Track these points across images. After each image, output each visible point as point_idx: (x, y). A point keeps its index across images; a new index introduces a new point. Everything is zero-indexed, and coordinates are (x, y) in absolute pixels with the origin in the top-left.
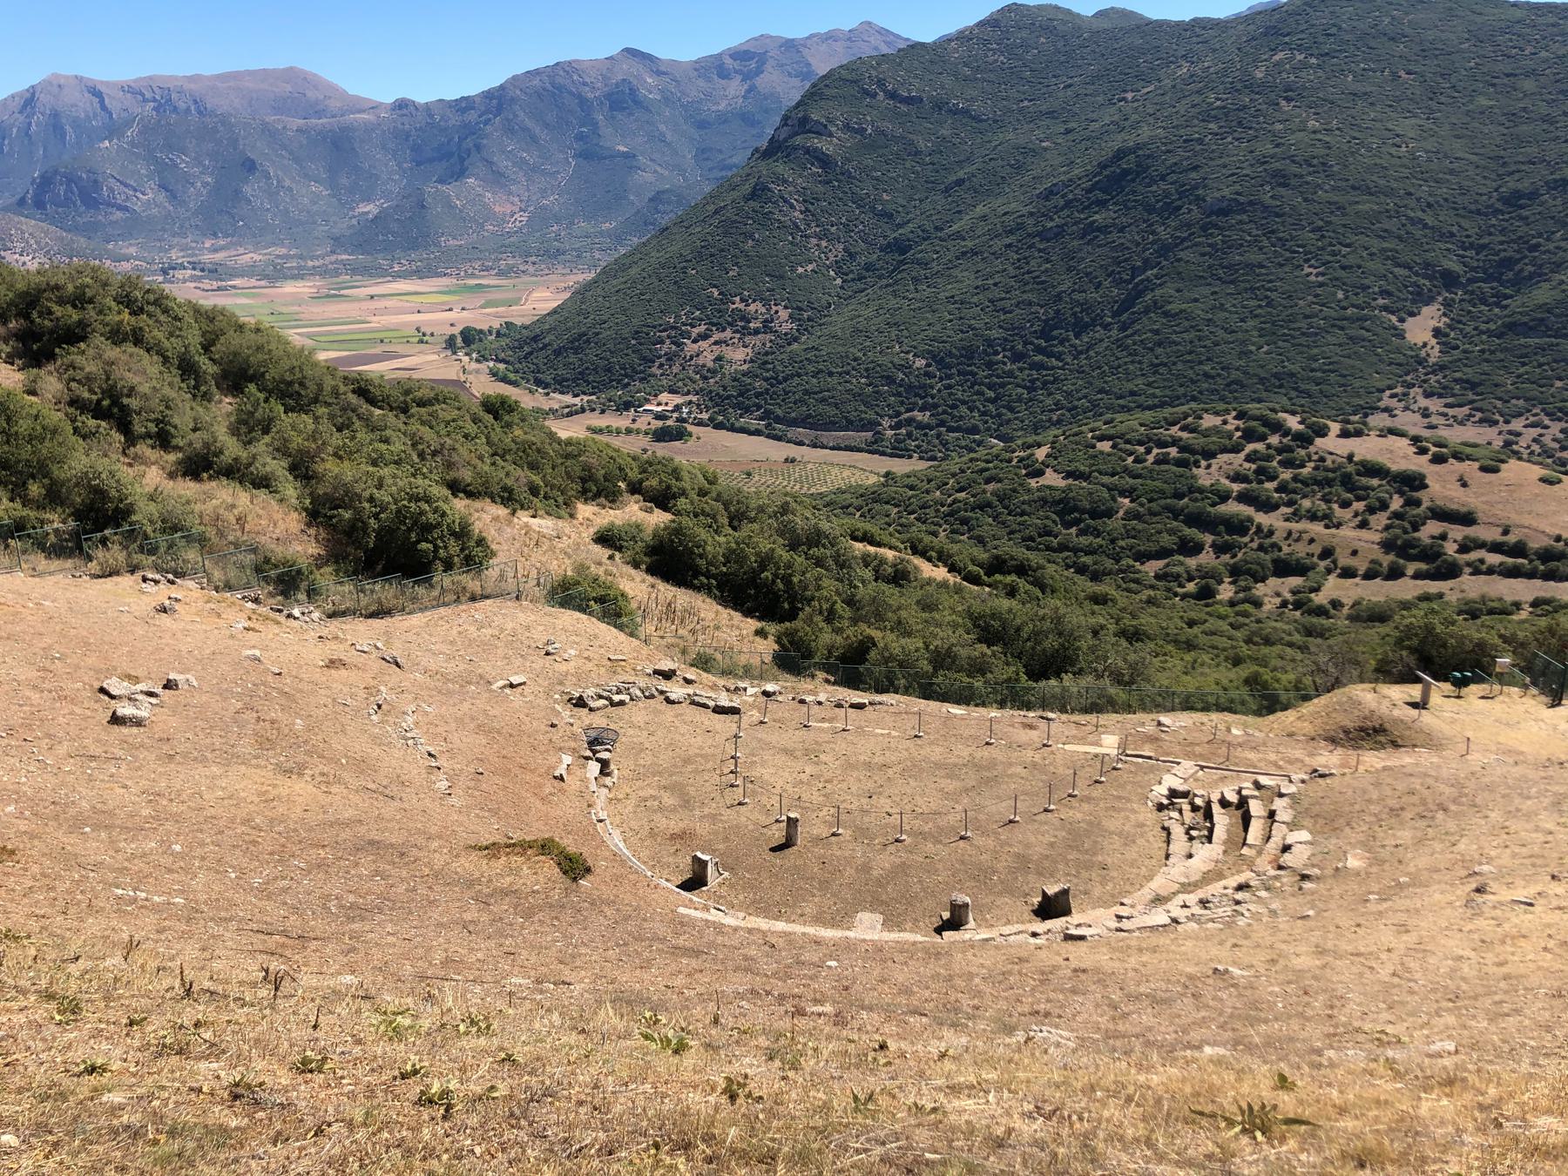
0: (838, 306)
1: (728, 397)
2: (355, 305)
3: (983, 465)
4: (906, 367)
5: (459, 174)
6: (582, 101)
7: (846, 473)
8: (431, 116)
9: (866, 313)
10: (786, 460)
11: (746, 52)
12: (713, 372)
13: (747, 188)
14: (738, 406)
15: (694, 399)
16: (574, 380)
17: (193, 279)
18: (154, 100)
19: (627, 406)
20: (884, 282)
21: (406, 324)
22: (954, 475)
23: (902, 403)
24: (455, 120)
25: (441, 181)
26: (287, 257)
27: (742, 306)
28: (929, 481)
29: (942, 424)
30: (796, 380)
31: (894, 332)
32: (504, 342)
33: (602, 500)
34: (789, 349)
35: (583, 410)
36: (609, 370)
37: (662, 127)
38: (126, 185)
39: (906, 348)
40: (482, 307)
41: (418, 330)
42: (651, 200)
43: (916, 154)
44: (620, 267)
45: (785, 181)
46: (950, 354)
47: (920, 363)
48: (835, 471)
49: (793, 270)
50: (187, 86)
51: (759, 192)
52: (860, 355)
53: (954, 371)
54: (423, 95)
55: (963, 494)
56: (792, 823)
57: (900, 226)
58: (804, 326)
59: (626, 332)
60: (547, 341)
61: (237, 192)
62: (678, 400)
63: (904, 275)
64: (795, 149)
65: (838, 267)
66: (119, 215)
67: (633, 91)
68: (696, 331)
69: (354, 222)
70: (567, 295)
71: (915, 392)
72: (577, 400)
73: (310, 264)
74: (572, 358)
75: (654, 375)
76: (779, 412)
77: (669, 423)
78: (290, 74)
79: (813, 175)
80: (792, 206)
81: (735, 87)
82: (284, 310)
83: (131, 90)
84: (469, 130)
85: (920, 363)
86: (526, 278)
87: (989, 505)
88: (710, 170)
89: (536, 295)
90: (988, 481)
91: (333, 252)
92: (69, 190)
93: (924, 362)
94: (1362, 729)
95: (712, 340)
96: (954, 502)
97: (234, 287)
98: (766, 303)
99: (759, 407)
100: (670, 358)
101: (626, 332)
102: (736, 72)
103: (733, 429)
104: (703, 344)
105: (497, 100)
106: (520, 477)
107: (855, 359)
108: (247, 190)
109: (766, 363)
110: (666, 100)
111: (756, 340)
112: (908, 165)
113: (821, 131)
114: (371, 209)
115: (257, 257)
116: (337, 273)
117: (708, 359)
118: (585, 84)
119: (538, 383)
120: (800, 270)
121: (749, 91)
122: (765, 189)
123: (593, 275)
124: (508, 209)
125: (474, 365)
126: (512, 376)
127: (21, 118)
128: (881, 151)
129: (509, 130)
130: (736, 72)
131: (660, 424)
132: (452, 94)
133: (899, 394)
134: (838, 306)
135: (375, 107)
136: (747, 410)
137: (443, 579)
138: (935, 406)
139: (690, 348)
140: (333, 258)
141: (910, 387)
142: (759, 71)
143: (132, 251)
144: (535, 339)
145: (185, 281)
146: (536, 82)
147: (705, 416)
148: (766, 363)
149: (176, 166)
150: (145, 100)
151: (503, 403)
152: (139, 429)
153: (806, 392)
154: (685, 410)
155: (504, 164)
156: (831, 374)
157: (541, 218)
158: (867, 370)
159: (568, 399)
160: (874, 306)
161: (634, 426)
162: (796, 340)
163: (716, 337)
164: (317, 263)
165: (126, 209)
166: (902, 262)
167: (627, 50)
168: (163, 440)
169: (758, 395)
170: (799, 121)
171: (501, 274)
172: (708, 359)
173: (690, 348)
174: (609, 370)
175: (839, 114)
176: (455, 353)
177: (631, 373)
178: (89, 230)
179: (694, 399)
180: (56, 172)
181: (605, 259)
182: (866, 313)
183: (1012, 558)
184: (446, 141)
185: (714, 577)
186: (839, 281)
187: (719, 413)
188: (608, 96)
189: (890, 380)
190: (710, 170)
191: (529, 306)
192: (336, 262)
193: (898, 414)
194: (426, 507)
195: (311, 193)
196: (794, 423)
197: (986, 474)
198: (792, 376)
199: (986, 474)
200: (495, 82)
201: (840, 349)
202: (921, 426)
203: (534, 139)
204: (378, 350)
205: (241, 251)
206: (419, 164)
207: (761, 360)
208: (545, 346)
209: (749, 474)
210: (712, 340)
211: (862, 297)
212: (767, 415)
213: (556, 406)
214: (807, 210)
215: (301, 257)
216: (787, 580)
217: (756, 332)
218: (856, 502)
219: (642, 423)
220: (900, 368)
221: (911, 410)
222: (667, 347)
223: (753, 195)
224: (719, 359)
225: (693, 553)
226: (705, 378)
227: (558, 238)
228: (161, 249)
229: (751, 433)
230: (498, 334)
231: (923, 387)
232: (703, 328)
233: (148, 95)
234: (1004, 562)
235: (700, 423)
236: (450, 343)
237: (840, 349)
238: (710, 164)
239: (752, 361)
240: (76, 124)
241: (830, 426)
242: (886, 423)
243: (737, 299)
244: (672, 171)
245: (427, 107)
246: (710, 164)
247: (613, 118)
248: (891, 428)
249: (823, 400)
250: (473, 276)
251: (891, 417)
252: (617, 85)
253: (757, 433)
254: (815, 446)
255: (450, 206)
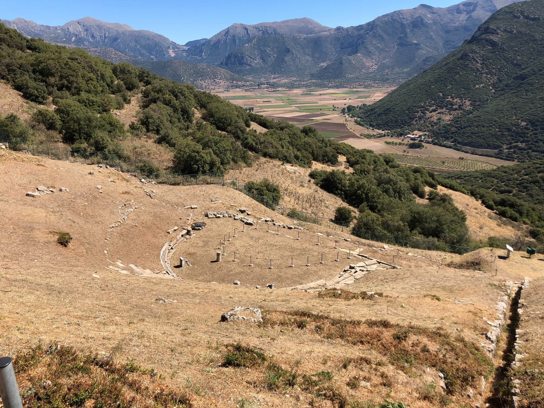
0: (491, 100)
1: (440, 133)
2: (315, 97)
3: (538, 165)
4: (517, 125)
5: (356, 52)
6: (402, 25)
7: (484, 165)
8: (348, 32)
9: (504, 103)
10: (460, 158)
11: (469, 3)
12: (436, 124)
13: (459, 56)
14: (444, 137)
15: (427, 133)
16: (383, 125)
17: (267, 88)
18: (262, 30)
19: (401, 135)
20: (513, 91)
21: (330, 104)
22: (524, 169)
23: (513, 139)
24: (356, 33)
25: (349, 55)
26: (295, 81)
27: (451, 100)
28: (513, 170)
29: (530, 148)
30: (469, 128)
31: (514, 111)
32: (362, 111)
33: (329, 163)
34: (468, 116)
35: (385, 136)
36: (396, 122)
37: (432, 33)
38: (251, 58)
39: (518, 118)
40: (356, 98)
41: (333, 106)
42: (424, 60)
43: (534, 41)
44: (407, 84)
45: (475, 52)
46: (538, 121)
47: (524, 124)
48: (479, 164)
49: (474, 86)
50: (272, 25)
51: (464, 56)
52: (497, 119)
53: (539, 127)
54: (346, 24)
55: (527, 177)
56: (218, 255)
57: (524, 69)
58: (475, 107)
59: (405, 108)
60: (376, 111)
61: (283, 59)
62: (421, 133)
63: (522, 89)
64: (482, 39)
65: (494, 85)
66: (248, 67)
67: (422, 20)
68: (431, 109)
69: (319, 69)
70: (386, 95)
71: (520, 135)
72: (383, 132)
73: (303, 83)
74: (384, 117)
75: (413, 124)
76: (460, 140)
77: (416, 142)
78: (304, 20)
79: (488, 49)
80: (477, 62)
81: (463, 17)
82: (292, 98)
83: (256, 27)
84: (361, 37)
85: (524, 124)
86: (373, 89)
87: (538, 182)
88: (449, 49)
89: (376, 94)
90: (539, 172)
91: (310, 79)
92: (235, 60)
93: (525, 123)
94: (473, 263)
95: (437, 112)
96: (522, 179)
97: (278, 91)
98: (461, 98)
99: (452, 138)
100: (420, 118)
101: (405, 108)
102: (464, 11)
103: (440, 145)
104: (434, 113)
105: (371, 26)
106: (292, 152)
107: (495, 121)
108: (286, 59)
109: (458, 121)
110: (435, 23)
111: (455, 113)
112: (530, 45)
113: (494, 32)
114: (324, 64)
115: (287, 81)
116: (310, 86)
117: (435, 119)
118: (404, 18)
119: (371, 125)
120: (477, 86)
121: (468, 18)
122: (467, 55)
123: (395, 88)
124: (371, 64)
125: (350, 119)
126: (362, 123)
127: (225, 37)
128: (519, 40)
129: (374, 36)
130: (464, 11)
131: (412, 142)
132: (356, 24)
133: (512, 136)
134: (491, 100)
135: (330, 30)
136: (447, 138)
137: (201, 177)
138: (528, 141)
139: (428, 114)
140: (310, 81)
141: (517, 133)
142: (474, 10)
143: (251, 78)
144: (372, 110)
145: (264, 88)
146: (386, 19)
147: (430, 140)
148: (458, 121)
149: (266, 51)
150: (260, 31)
151: (310, 129)
152: (151, 128)
153: (472, 133)
154: (423, 137)
155: (371, 48)
156: (484, 127)
157: (382, 67)
158: (499, 125)
159: (380, 131)
160: (507, 100)
161: (402, 142)
162: (471, 113)
163: (439, 111)
164: (305, 83)
165: (250, 65)
166: (522, 84)
167: (422, 5)
168: (158, 132)
169: (452, 133)
170: (485, 29)
171: (366, 87)
172: (435, 119)
173: (428, 114)
174: (396, 122)
175: (502, 26)
176: (344, 114)
177: (404, 123)
178: (238, 72)
179: (427, 133)
180: (232, 54)
181: (402, 81)
182: (504, 103)
183: (509, 200)
184: (352, 41)
185: (344, 191)
186: (493, 91)
187: (435, 139)
188: (412, 23)
189: (509, 130)
190: (449, 49)
191: (373, 98)
192: (311, 82)
193: (511, 143)
194: (197, 154)
195: (306, 59)
196: (466, 144)
197: (539, 169)
198: (468, 127)
199: (539, 169)
200: (371, 19)
201: (489, 117)
202: (520, 149)
203: (383, 39)
204: (319, 113)
205: (282, 79)
206: (342, 49)
207: (456, 120)
208: (375, 112)
209: (443, 162)
210: (437, 112)
211: (502, 97)
212: (455, 141)
213: (375, 134)
214: (483, 63)
215: (300, 81)
216: (367, 194)
217: (456, 109)
218: (481, 176)
219: (406, 142)
220: (514, 125)
221: (517, 142)
222: (420, 114)
223: (461, 58)
224: (439, 119)
225: (336, 182)
226: (432, 126)
227: (387, 74)
228: (259, 78)
229: (447, 147)
230: (360, 108)
231: (524, 133)
232: (434, 107)
233: (261, 29)
234: (506, 201)
235: (428, 142)
236: (343, 111)
237: (489, 117)
238: (449, 46)
239: (452, 120)
240: (240, 39)
241: (478, 147)
242: (505, 147)
243: (450, 97)
244: (432, 49)
245: (347, 29)
246: (449, 46)
247: (413, 30)
248: (507, 149)
249: (479, 136)
250: (355, 88)
251: (507, 144)
252: (416, 18)
253: (450, 147)
254: (473, 154)
255: (351, 63)
